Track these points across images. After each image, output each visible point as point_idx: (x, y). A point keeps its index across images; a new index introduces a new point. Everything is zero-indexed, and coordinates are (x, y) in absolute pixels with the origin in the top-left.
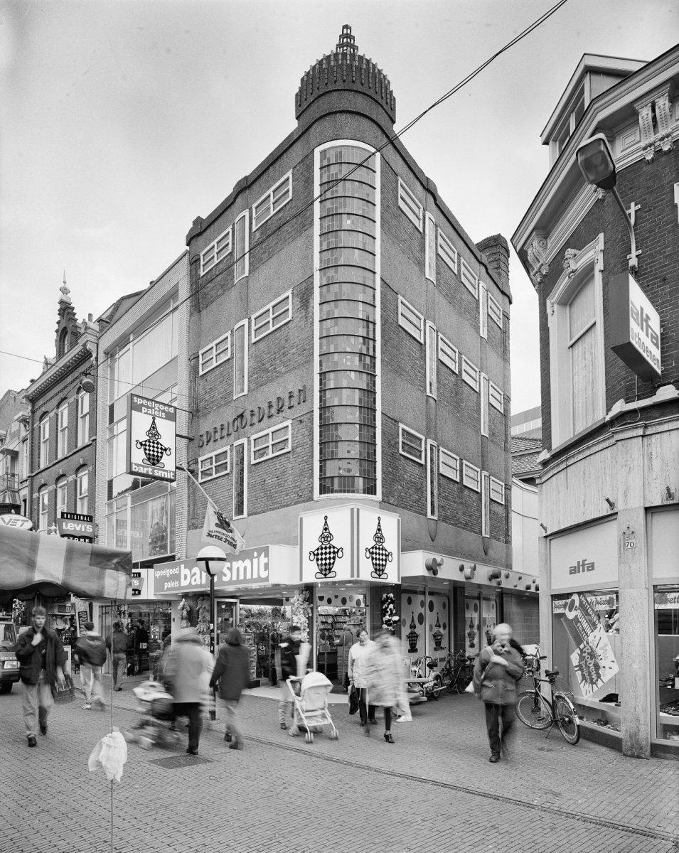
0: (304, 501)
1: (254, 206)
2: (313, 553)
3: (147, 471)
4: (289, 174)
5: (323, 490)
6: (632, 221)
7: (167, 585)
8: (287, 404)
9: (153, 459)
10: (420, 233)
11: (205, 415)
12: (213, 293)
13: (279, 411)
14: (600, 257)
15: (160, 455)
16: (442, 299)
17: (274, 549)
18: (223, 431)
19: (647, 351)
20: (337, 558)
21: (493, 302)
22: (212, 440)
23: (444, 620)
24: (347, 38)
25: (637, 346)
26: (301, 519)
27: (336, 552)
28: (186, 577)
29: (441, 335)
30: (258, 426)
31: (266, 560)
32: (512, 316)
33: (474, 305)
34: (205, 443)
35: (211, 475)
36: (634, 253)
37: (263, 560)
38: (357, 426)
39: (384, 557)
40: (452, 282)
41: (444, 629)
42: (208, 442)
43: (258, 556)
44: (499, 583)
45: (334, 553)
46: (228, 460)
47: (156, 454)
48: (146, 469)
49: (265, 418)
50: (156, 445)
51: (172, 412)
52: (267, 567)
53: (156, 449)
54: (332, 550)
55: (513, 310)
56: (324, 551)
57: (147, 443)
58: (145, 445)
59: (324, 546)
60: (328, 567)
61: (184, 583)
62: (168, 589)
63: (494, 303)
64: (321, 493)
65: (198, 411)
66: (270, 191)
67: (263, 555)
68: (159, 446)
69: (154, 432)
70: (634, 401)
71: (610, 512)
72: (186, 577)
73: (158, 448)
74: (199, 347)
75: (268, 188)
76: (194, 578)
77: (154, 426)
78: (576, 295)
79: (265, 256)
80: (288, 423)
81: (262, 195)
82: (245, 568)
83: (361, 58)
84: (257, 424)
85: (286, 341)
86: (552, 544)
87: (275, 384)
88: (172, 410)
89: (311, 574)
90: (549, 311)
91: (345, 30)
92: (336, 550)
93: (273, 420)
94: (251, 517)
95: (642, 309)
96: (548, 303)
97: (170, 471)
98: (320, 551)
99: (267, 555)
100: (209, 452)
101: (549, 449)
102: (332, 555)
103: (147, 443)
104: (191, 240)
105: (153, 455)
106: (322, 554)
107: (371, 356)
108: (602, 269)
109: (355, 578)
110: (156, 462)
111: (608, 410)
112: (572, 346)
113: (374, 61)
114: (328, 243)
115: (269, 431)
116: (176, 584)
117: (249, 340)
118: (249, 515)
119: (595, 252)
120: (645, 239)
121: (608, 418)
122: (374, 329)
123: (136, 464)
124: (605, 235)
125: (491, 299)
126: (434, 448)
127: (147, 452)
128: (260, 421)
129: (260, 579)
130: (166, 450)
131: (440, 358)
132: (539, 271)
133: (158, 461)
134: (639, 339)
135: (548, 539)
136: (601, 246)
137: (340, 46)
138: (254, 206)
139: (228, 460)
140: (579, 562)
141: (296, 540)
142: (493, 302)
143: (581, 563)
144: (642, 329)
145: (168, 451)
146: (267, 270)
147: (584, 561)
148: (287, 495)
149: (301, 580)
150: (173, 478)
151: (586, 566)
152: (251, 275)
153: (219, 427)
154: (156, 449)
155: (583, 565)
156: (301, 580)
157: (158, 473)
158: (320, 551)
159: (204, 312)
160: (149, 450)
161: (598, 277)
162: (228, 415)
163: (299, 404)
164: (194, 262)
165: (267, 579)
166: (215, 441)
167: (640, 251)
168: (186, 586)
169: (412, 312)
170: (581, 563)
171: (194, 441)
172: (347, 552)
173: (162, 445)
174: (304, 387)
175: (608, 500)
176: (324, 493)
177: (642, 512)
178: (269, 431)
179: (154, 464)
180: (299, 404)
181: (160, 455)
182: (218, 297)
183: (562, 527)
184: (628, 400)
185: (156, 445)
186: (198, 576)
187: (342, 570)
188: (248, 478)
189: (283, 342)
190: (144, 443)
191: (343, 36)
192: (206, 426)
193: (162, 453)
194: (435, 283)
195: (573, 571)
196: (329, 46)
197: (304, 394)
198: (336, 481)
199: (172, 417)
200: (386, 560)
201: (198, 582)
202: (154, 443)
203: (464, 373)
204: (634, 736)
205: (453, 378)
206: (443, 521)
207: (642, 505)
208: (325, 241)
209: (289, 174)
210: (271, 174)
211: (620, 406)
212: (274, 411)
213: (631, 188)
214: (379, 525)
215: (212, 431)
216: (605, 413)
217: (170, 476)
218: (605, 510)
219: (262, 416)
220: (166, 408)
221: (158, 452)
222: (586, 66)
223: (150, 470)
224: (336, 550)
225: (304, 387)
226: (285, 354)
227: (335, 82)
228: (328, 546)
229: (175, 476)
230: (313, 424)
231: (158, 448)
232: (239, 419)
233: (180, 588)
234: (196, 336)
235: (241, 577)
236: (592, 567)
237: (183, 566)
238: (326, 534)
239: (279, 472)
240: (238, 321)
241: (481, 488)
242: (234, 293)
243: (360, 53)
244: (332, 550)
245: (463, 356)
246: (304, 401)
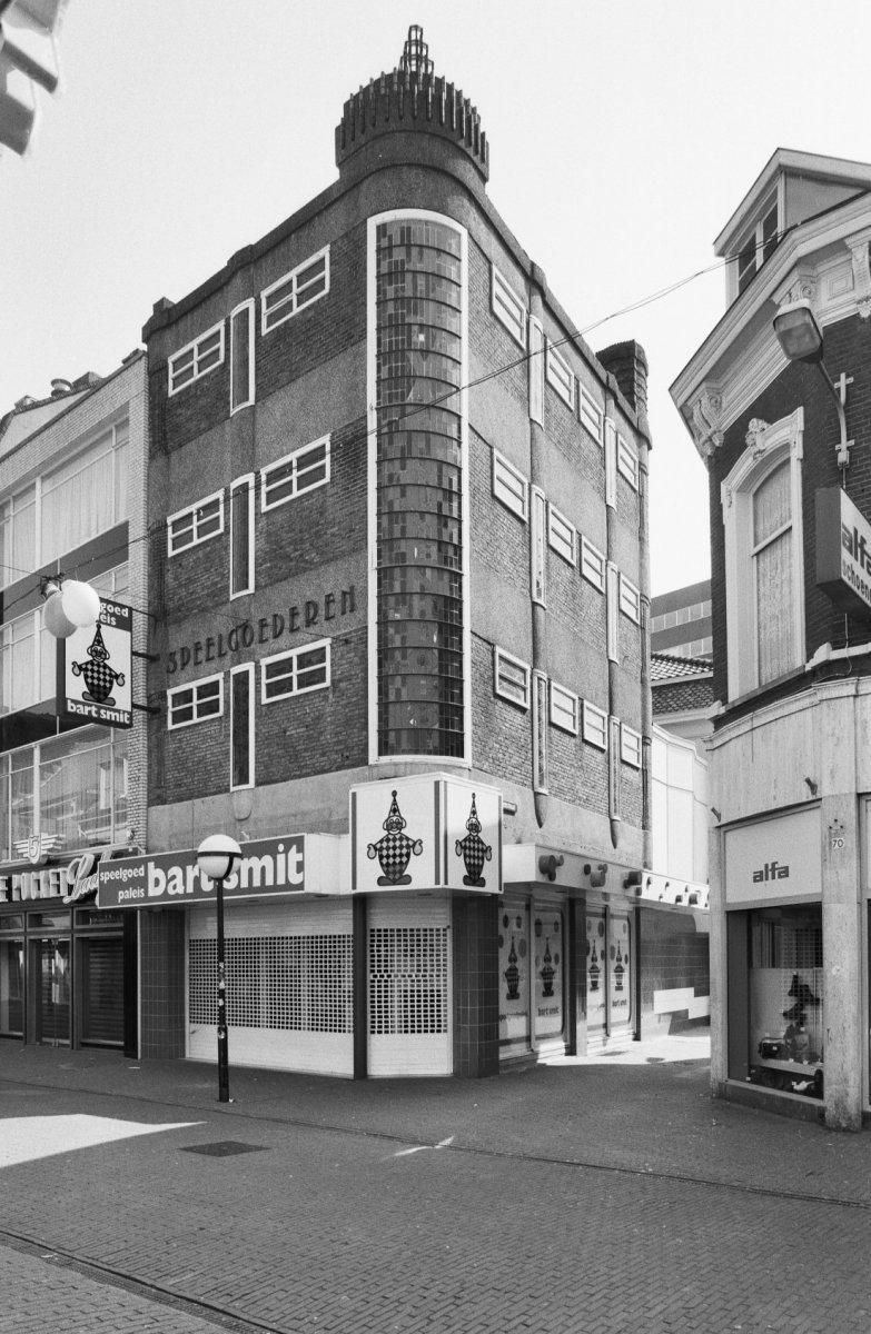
0: (354, 766)
1: (264, 294)
2: (374, 847)
3: (90, 712)
4: (325, 252)
5: (384, 749)
6: (843, 398)
7: (122, 895)
8: (322, 612)
9: (99, 693)
10: (571, 411)
11: (178, 621)
12: (192, 425)
13: (310, 622)
14: (799, 440)
15: (108, 685)
16: (553, 451)
17: (312, 841)
18: (211, 648)
19: (862, 587)
20: (412, 854)
21: (625, 448)
22: (192, 662)
23: (556, 949)
24: (415, 48)
25: (849, 583)
26: (354, 795)
27: (413, 846)
28: (157, 882)
29: (551, 507)
30: (272, 644)
31: (299, 857)
32: (650, 470)
33: (598, 457)
34: (179, 667)
35: (191, 718)
36: (844, 444)
37: (294, 856)
38: (436, 652)
39: (480, 854)
40: (568, 421)
41: (557, 962)
42: (184, 665)
43: (286, 851)
44: (638, 892)
45: (408, 847)
46: (221, 696)
47: (102, 683)
48: (87, 709)
49: (285, 632)
50: (102, 670)
51: (127, 615)
52: (300, 867)
53: (102, 677)
54: (404, 843)
55: (653, 459)
56: (391, 844)
57: (89, 667)
58: (86, 670)
59: (391, 837)
60: (398, 868)
61: (154, 892)
62: (124, 901)
63: (627, 451)
64: (380, 754)
65: (165, 613)
66: (292, 275)
67: (294, 847)
68: (108, 671)
69: (99, 648)
70: (843, 647)
71: (811, 798)
72: (157, 882)
73: (105, 674)
74: (167, 510)
75: (289, 269)
76: (172, 883)
77: (98, 639)
78: (764, 483)
79: (284, 377)
80: (326, 643)
81: (277, 278)
82: (263, 869)
83: (440, 82)
84: (271, 641)
85: (321, 514)
86: (727, 839)
87: (302, 578)
88: (125, 613)
89: (370, 877)
90: (724, 500)
91: (413, 33)
92: (411, 843)
93: (299, 636)
94: (261, 788)
95: (856, 531)
96: (724, 487)
97: (124, 712)
98: (385, 845)
99: (300, 850)
100: (188, 681)
101: (725, 701)
102: (404, 851)
103: (89, 667)
104: (151, 332)
105: (98, 685)
106: (388, 848)
107: (455, 546)
108: (801, 457)
109: (442, 885)
110: (102, 696)
111: (809, 656)
112: (757, 554)
113: (448, 80)
114: (390, 368)
115: (293, 653)
116: (140, 893)
117: (257, 506)
118: (258, 784)
119: (790, 430)
120: (858, 426)
121: (808, 667)
122: (460, 504)
123: (73, 701)
124: (805, 410)
125: (622, 445)
126: (543, 684)
127: (90, 680)
128: (276, 636)
129: (288, 886)
130: (117, 677)
131: (552, 543)
132: (710, 439)
133: (106, 695)
134: (853, 572)
135: (723, 829)
136: (800, 425)
137: (406, 57)
138: (264, 294)
139: (221, 696)
140: (766, 866)
141: (341, 824)
142: (625, 448)
143: (770, 867)
144: (856, 559)
145: (120, 680)
146: (283, 404)
147: (774, 864)
148: (323, 755)
149: (354, 887)
150: (127, 722)
151: (777, 872)
152: (259, 404)
153: (203, 641)
154: (102, 677)
155: (774, 869)
156: (354, 887)
157: (106, 715)
158: (385, 845)
159: (174, 456)
160: (92, 678)
161: (795, 471)
162: (220, 624)
163: (343, 613)
164: (157, 374)
165: (301, 886)
166: (197, 664)
167: (852, 442)
168: (159, 896)
169: (511, 473)
170: (770, 867)
171: (157, 661)
172: (429, 845)
173: (111, 670)
174: (352, 588)
175: (808, 781)
176: (386, 754)
177: (853, 800)
178: (293, 653)
179: (99, 701)
180: (343, 613)
181: (108, 685)
182: (200, 432)
183: (743, 815)
184: (836, 646)
185: (102, 670)
186: (179, 881)
187: (421, 874)
188: (256, 725)
189: (315, 515)
190: (84, 666)
191: (409, 43)
192: (179, 639)
193: (111, 682)
194: (543, 425)
195: (759, 877)
196: (389, 62)
197: (351, 599)
198: (404, 735)
199: (125, 624)
200: (483, 859)
201: (180, 890)
202: (99, 666)
203: (584, 565)
204: (839, 1104)
205: (568, 572)
206: (555, 795)
207: (853, 791)
208: (384, 365)
209: (325, 252)
210: (293, 247)
211: (824, 653)
212: (300, 621)
213: (841, 353)
214: (474, 806)
215: (190, 646)
216: (804, 658)
217: (124, 718)
218: (804, 794)
219: (280, 627)
220: (117, 609)
221: (105, 681)
222: (780, 166)
223: (94, 709)
224: (411, 843)
225: (352, 588)
226: (318, 535)
227: (401, 118)
228: (398, 837)
229: (131, 719)
230: (366, 647)
231: (105, 674)
232: (240, 632)
233: (147, 898)
234: (161, 493)
235: (257, 883)
236: (785, 872)
237: (151, 865)
238: (394, 818)
239: (309, 719)
240: (236, 477)
241: (532, 703)
242: (228, 428)
243: (438, 73)
244: (404, 843)
245: (583, 537)
246: (352, 611)
